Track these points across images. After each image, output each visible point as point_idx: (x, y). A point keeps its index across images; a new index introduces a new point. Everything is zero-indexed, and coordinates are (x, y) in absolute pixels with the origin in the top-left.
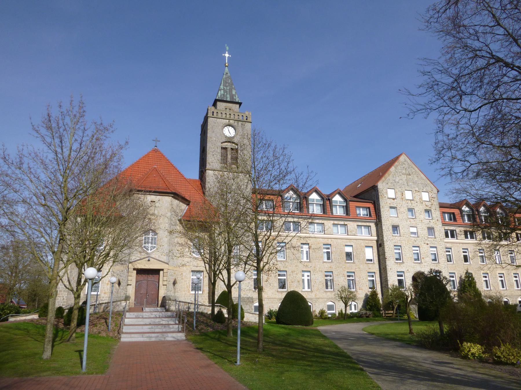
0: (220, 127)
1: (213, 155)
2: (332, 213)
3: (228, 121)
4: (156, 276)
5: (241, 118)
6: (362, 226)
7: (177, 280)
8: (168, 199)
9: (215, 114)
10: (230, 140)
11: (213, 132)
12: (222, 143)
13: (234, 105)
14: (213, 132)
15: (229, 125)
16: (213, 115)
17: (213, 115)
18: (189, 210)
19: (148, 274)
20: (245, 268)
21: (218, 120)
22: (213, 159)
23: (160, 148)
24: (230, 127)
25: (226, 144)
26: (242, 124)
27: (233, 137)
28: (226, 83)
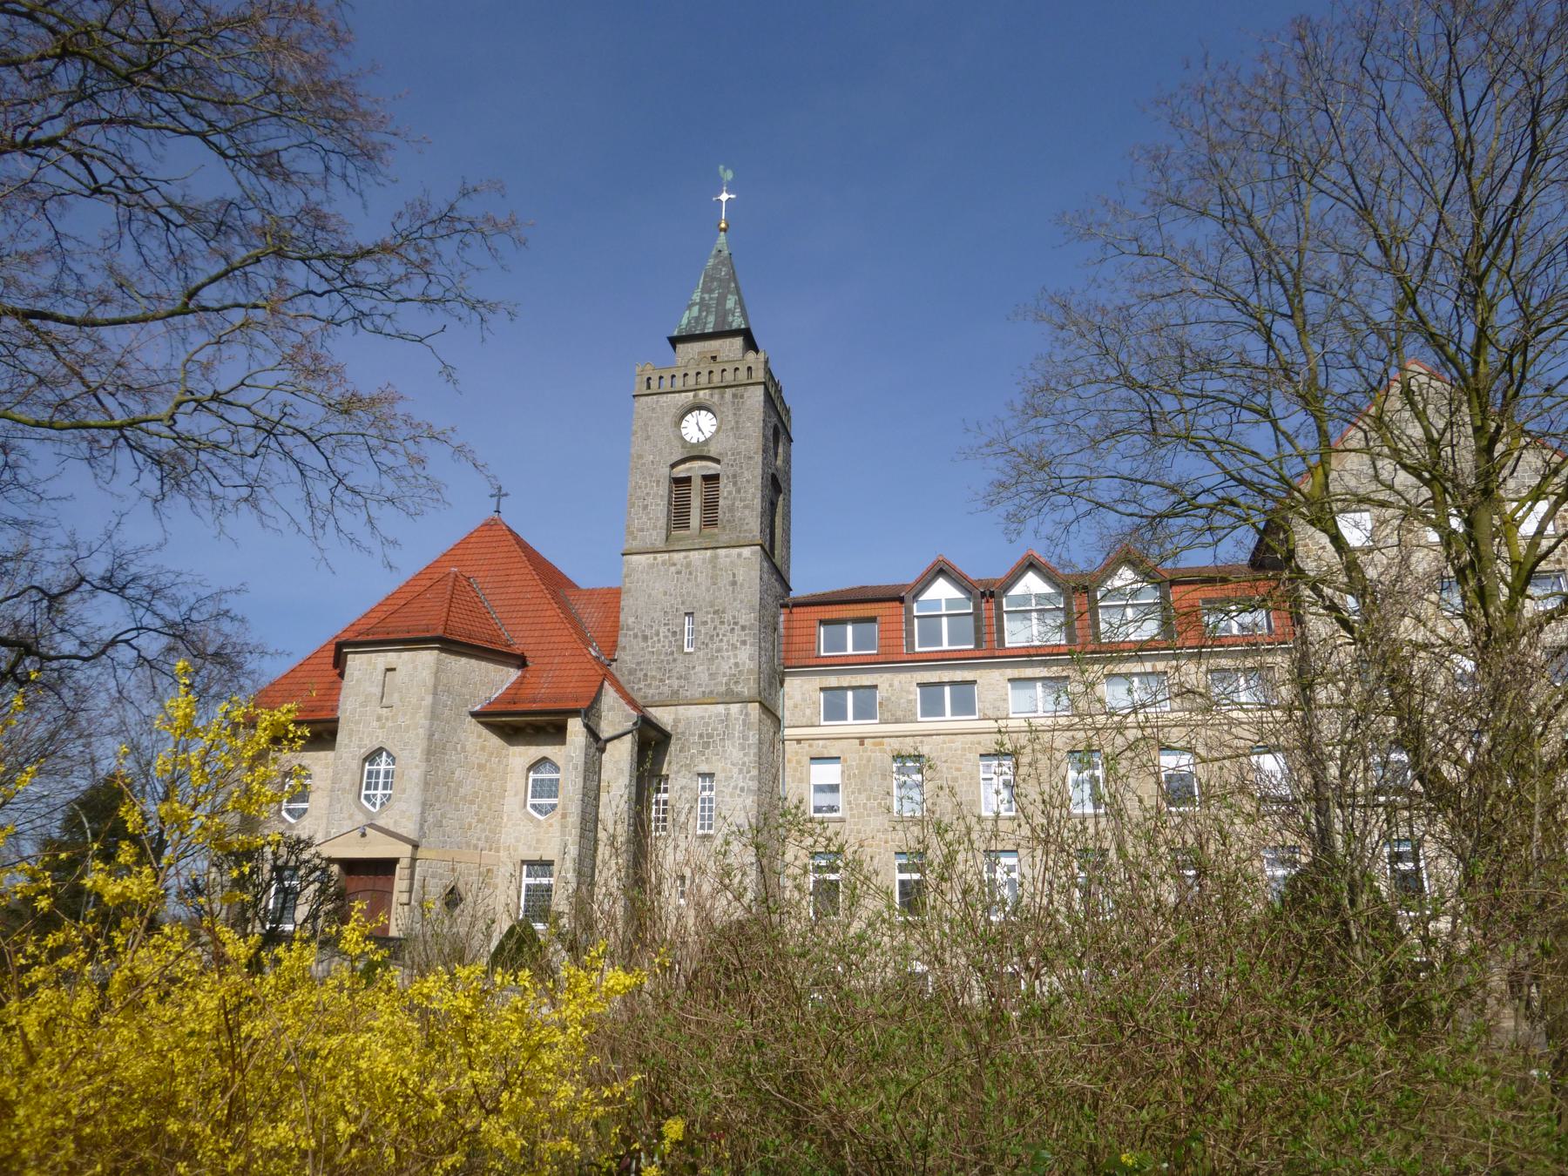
0: (667, 420)
1: (645, 507)
2: (1001, 640)
3: (691, 394)
4: (380, 882)
5: (729, 376)
6: (941, 684)
7: (461, 887)
8: (427, 659)
9: (654, 384)
10: (697, 454)
11: (648, 438)
12: (673, 466)
13: (728, 341)
14: (648, 438)
15: (700, 407)
16: (649, 387)
17: (649, 387)
18: (519, 683)
19: (376, 874)
20: (1412, 738)
21: (664, 398)
22: (645, 518)
23: (508, 518)
24: (703, 413)
25: (688, 465)
26: (734, 396)
27: (707, 441)
28: (713, 279)
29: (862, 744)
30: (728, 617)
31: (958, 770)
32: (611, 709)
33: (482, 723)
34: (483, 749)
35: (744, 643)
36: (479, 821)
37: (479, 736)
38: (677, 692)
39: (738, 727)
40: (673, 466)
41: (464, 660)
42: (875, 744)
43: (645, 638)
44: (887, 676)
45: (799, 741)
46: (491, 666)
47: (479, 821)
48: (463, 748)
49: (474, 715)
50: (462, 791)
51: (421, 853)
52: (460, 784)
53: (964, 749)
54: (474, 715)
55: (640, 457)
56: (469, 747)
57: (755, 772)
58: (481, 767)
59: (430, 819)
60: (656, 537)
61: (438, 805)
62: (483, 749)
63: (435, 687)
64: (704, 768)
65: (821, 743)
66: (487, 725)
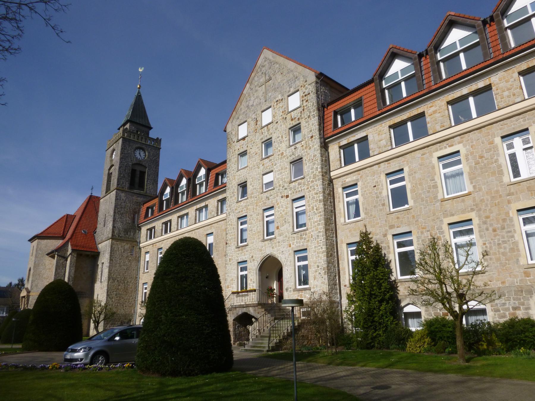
34: (51, 264)
41: (46, 241)
46: (54, 241)
49: (48, 254)
50: (44, 276)
51: (31, 294)
54: (48, 254)
56: (47, 264)
59: (34, 285)
62: (51, 264)
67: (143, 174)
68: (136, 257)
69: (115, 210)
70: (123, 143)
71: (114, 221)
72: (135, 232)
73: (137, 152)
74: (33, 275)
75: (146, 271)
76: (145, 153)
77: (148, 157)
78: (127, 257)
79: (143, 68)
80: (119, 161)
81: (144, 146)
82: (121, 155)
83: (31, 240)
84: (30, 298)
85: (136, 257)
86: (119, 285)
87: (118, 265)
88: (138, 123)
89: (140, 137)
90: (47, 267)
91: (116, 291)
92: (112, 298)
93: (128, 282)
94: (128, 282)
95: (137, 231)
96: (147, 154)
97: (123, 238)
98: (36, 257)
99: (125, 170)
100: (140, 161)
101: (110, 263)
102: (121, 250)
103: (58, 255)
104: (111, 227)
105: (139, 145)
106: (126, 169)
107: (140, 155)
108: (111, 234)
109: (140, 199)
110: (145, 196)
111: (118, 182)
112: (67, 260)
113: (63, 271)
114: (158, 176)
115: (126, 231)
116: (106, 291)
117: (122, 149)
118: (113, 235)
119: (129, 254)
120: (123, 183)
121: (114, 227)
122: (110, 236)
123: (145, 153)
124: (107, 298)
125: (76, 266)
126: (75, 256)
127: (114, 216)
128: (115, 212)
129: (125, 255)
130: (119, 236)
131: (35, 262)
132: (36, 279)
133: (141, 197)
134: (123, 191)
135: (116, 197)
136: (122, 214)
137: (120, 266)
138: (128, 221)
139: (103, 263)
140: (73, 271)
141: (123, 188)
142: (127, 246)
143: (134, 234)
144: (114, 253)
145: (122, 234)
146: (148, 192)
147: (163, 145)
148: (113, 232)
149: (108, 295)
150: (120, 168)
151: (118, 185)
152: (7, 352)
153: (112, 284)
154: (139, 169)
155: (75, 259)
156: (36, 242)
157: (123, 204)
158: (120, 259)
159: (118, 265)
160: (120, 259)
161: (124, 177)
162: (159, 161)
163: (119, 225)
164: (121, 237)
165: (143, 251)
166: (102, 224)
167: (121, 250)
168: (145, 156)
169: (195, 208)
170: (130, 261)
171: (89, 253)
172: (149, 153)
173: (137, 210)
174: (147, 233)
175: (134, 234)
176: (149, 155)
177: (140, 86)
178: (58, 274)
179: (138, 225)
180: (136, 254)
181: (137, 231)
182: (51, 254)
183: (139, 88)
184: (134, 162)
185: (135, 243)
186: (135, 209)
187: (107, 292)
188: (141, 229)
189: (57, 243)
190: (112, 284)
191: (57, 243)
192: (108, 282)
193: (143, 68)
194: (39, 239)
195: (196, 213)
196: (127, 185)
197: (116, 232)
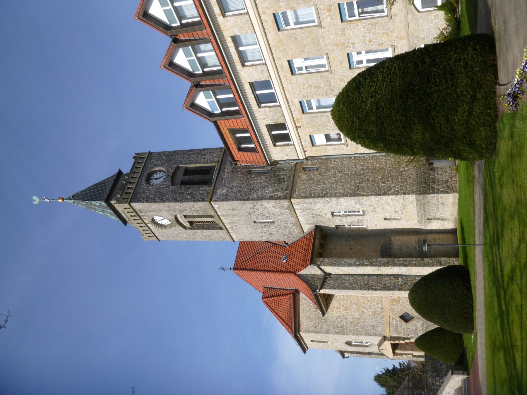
12: (185, 228)
13: (218, 61)
29: (300, 127)
30: (251, 211)
31: (304, 85)
32: (310, 271)
33: (327, 310)
34: (338, 308)
35: (262, 205)
36: (370, 308)
37: (333, 310)
38: (294, 224)
39: (306, 205)
40: (185, 228)
41: (301, 320)
42: (299, 122)
43: (271, 234)
44: (259, 121)
45: (305, 152)
46: (301, 307)
47: (370, 308)
48: (340, 317)
49: (324, 314)
50: (359, 317)
51: (388, 335)
52: (355, 318)
53: (291, 83)
54: (324, 314)
55: (186, 238)
56: (338, 315)
57: (327, 199)
58: (346, 309)
59: (373, 331)
60: (222, 233)
61: (366, 328)
62: (338, 308)
63: (316, 332)
64: (330, 215)
65: (303, 143)
66: (327, 307)
67: (187, 172)
68: (321, 163)
69: (243, 200)
70: (138, 201)
71: (261, 199)
72: (280, 169)
73: (154, 182)
74: (357, 334)
75: (327, 68)
76: (155, 172)
77: (162, 166)
78: (321, 175)
79: (35, 198)
80: (167, 204)
81: (145, 174)
82: (157, 202)
83: (304, 348)
84: (396, 335)
85: (321, 163)
86: (368, 180)
87: (334, 186)
88: (113, 190)
89: (131, 180)
90: (343, 313)
91: (378, 183)
92: (389, 187)
93: (362, 169)
94: (362, 169)
95: (279, 166)
96: (157, 169)
97: (290, 184)
98: (328, 332)
99: (181, 194)
100: (168, 176)
101: (331, 196)
102: (309, 184)
103: (321, 288)
104: (272, 202)
105: (143, 181)
106: (179, 193)
107: (159, 179)
108: (282, 201)
109: (228, 168)
110: (222, 163)
111: (199, 201)
112: (330, 274)
113: (347, 278)
114: (192, 150)
115: (279, 180)
116: (378, 198)
117: (148, 201)
118: (285, 198)
119: (316, 172)
120: (201, 194)
121: (271, 198)
122: (285, 203)
123: (155, 172)
124: (389, 194)
125: (340, 257)
126: (321, 259)
127: (253, 199)
128: (248, 200)
129: (318, 177)
130: (286, 190)
131: (336, 333)
132: (363, 328)
133: (225, 168)
134: (214, 192)
135: (223, 200)
136: (250, 189)
137: (336, 182)
138: (263, 181)
139: (333, 214)
140: (346, 260)
141: (208, 193)
142: (303, 176)
143: (284, 170)
144: (315, 193)
145: (284, 185)
146: (216, 160)
147: (145, 150)
148: (279, 198)
149: (385, 194)
150: (177, 201)
151: (203, 200)
152: (462, 2)
153: (366, 190)
154: (180, 177)
155: (326, 259)
156: (307, 337)
157: (234, 190)
158: (325, 183)
159: (334, 186)
160: (325, 183)
161: (191, 193)
162: (169, 152)
163: (268, 192)
164: (288, 186)
165: (311, 152)
166: (272, 229)
167: (309, 184)
168: (160, 171)
169: (220, 19)
170: (327, 170)
171: (317, 241)
172: (155, 166)
173: (244, 170)
174: (279, 146)
175: (284, 170)
176: (159, 166)
177: (59, 198)
178: (352, 285)
179: (268, 165)
180: (316, 164)
181: (279, 166)
182: (324, 303)
183: (63, 199)
184: (169, 183)
185: (298, 167)
186: (243, 173)
187: (380, 195)
188: (275, 161)
189: (307, 305)
190: (366, 190)
191: (307, 305)
192: (363, 195)
193: (35, 198)
194: (299, 331)
195: (230, 16)
196: (204, 188)
197: (280, 194)
